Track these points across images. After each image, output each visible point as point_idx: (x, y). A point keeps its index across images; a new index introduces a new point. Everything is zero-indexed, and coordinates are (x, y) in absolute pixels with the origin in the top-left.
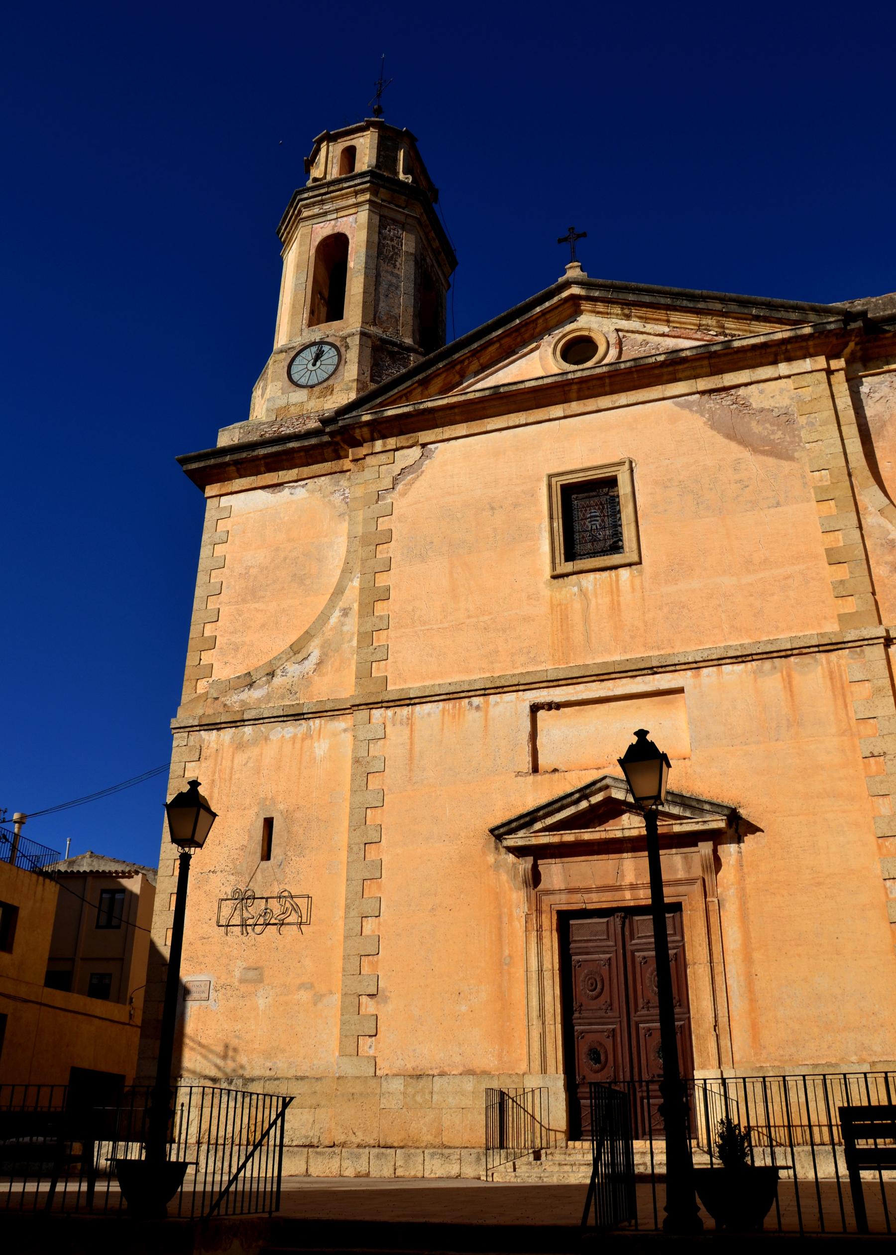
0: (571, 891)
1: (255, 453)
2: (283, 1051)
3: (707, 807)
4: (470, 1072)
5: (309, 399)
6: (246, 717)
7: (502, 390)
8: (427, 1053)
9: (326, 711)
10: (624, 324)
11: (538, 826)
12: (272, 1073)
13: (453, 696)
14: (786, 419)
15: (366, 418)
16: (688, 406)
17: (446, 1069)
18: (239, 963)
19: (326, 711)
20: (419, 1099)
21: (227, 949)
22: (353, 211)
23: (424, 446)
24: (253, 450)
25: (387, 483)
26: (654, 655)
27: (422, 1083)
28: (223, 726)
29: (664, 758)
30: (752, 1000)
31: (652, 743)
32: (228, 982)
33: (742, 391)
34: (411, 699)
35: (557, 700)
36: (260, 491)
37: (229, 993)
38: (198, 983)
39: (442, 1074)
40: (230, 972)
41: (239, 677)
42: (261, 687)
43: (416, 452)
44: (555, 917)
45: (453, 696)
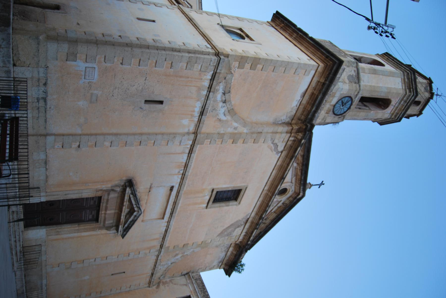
0: (108, 200)
1: (321, 94)
3: (125, 233)
4: (47, 177)
5: (331, 105)
6: (211, 93)
10: (282, 202)
11: (131, 196)
12: (48, 109)
13: (186, 166)
15: (303, 141)
18: (100, 92)
20: (37, 164)
22: (392, 112)
24: (323, 94)
25: (276, 141)
26: (176, 215)
28: (212, 82)
30: (66, 239)
33: (243, 226)
34: (191, 154)
35: (173, 193)
36: (306, 87)
38: (93, 74)
39: (46, 169)
41: (230, 88)
42: (222, 97)
43: (281, 148)
44: (99, 221)
45: (186, 166)
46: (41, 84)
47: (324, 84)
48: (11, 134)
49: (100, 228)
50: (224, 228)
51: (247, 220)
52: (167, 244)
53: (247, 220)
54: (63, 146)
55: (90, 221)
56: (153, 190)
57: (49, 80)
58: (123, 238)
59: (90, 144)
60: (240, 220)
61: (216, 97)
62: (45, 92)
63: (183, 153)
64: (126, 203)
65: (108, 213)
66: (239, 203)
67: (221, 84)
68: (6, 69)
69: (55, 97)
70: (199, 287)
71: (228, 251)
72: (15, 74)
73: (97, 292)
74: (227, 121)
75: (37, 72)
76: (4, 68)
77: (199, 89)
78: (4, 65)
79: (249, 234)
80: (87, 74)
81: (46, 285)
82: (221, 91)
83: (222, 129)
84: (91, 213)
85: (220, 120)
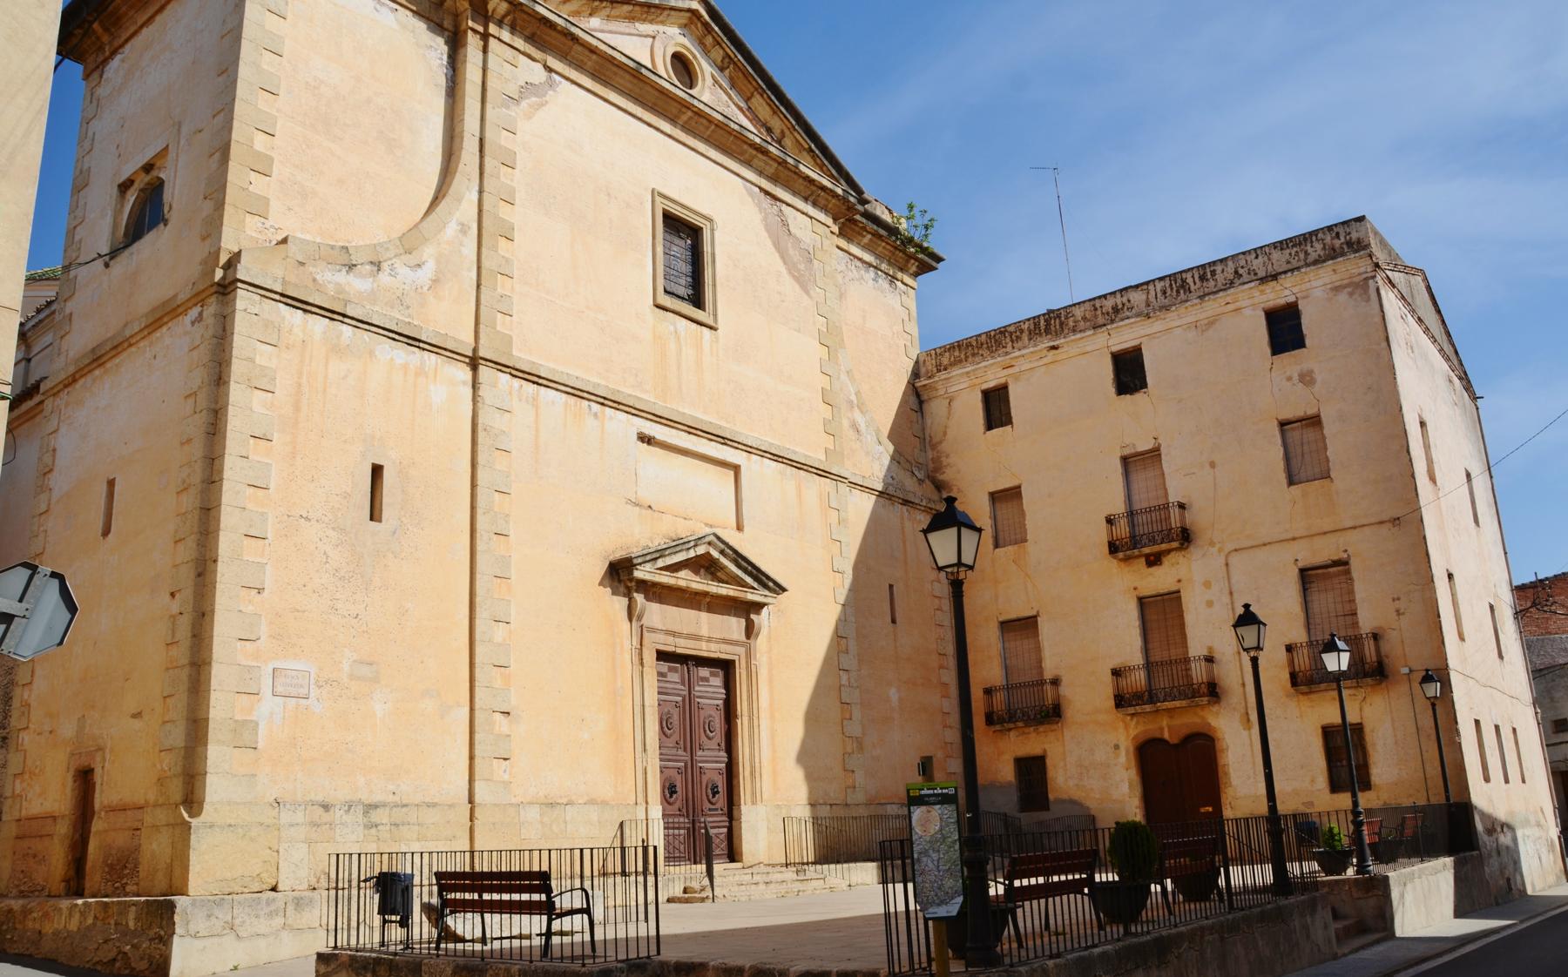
4: (592, 802)
7: (643, 71)
11: (660, 563)
12: (396, 798)
13: (577, 393)
14: (809, 256)
16: (751, 194)
23: (550, 70)
33: (784, 207)
41: (333, 247)
45: (577, 393)
46: (326, 817)
47: (875, 235)
49: (749, 655)
51: (767, 193)
52: (817, 457)
53: (767, 193)
55: (729, 684)
56: (646, 496)
57: (312, 797)
58: (784, 590)
59: (498, 683)
60: (765, 219)
62: (350, 806)
64: (686, 579)
65: (709, 632)
67: (318, 277)
68: (290, 908)
73: (941, 667)
77: (336, 350)
79: (812, 193)
80: (294, 692)
82: (342, 278)
84: (707, 680)
85: (436, 281)
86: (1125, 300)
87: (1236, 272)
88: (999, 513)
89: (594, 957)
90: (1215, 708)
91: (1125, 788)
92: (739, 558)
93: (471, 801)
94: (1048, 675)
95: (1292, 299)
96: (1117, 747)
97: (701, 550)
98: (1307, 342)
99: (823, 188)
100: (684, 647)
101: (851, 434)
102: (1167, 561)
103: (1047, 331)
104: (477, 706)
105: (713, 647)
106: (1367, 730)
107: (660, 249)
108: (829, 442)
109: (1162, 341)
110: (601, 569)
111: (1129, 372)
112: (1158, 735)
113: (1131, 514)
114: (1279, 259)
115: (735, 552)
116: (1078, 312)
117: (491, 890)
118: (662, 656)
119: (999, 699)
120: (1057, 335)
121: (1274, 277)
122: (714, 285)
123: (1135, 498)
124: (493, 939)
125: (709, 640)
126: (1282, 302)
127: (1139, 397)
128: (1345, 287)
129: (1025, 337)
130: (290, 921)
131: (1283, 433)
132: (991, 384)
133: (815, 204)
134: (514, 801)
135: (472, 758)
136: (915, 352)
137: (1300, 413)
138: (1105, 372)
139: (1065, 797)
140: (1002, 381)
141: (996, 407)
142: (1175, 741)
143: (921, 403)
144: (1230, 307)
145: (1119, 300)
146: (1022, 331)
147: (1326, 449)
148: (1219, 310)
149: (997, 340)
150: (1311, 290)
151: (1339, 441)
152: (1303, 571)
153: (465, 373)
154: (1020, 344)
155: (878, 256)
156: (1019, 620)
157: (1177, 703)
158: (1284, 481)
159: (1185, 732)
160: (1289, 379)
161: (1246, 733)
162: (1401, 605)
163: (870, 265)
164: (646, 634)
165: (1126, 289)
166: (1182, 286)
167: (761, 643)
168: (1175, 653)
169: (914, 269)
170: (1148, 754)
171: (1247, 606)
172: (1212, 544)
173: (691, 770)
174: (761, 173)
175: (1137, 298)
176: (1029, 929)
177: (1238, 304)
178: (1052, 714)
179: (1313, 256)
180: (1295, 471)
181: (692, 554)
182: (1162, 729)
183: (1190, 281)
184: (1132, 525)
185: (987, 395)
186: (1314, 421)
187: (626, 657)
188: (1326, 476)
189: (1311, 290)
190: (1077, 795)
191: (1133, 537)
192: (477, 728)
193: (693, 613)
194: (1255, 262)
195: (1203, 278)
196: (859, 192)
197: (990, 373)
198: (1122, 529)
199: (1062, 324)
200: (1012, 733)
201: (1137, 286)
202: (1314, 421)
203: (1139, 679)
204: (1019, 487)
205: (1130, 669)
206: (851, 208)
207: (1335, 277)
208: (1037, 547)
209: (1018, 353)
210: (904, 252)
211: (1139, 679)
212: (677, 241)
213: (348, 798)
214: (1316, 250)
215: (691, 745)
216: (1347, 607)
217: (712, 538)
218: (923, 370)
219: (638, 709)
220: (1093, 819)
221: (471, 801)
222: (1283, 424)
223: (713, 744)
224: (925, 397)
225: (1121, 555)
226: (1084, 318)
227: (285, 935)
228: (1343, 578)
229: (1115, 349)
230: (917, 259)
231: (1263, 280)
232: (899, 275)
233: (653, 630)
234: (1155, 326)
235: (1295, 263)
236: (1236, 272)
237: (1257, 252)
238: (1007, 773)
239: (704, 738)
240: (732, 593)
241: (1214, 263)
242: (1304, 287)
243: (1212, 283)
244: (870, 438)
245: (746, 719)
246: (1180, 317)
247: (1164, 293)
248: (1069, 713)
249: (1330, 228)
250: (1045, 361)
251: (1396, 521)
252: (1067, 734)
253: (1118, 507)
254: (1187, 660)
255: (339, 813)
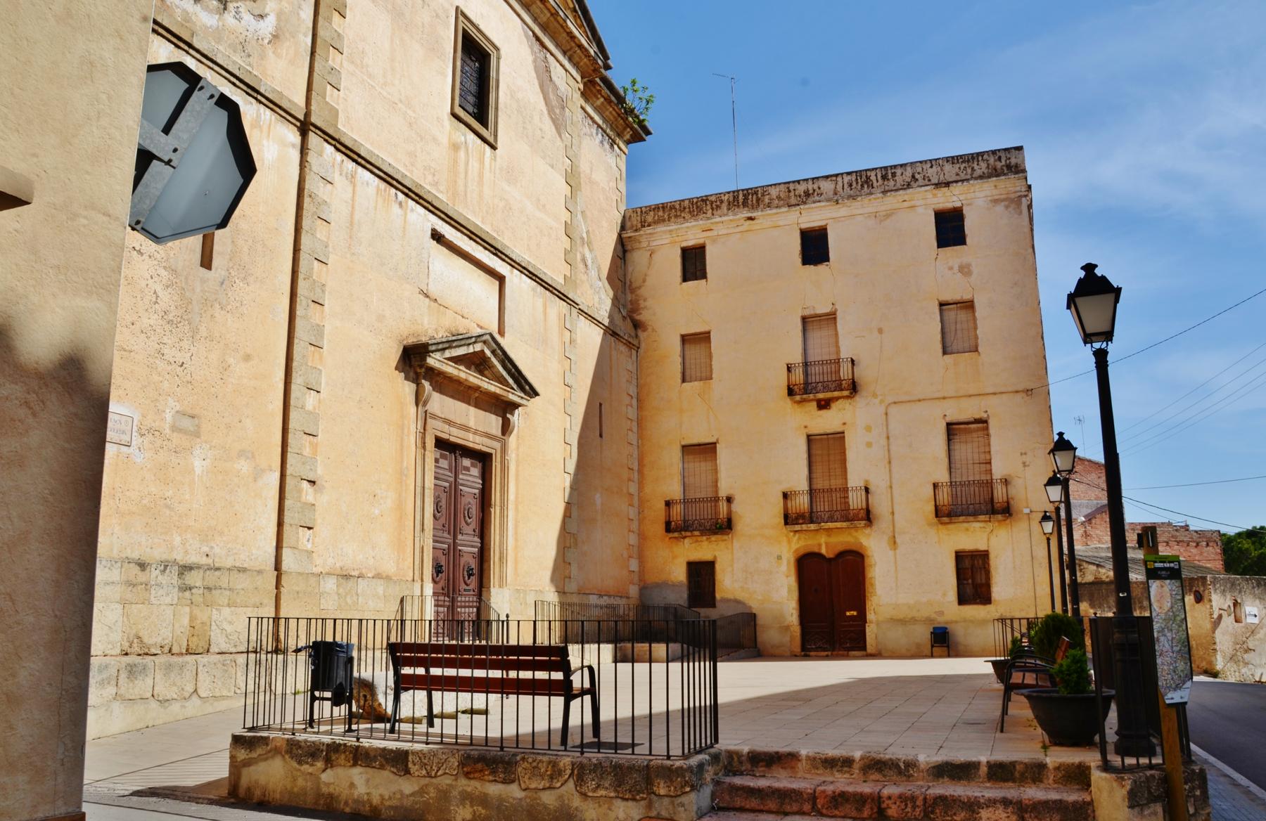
2: (221, 533)
4: (378, 576)
8: (352, 554)
9: (280, 107)
11: (448, 354)
12: (209, 561)
13: (388, 178)
16: (527, 36)
17: (364, 571)
19: (280, 107)
21: (156, 378)
27: (351, 583)
29: (1117, 292)
31: (1103, 278)
32: (156, 425)
33: (548, 55)
34: (359, 156)
37: (159, 442)
40: (160, 412)
45: (388, 178)
46: (142, 577)
48: (426, 664)
49: (504, 450)
50: (546, 112)
51: (538, 39)
52: (557, 279)
53: (538, 39)
54: (309, 528)
55: (486, 476)
56: (434, 290)
57: (129, 553)
58: (537, 394)
59: (307, 451)
60: (535, 61)
61: (207, 28)
62: (165, 566)
63: (352, 178)
64: (461, 373)
65: (474, 425)
66: (497, 49)
68: (123, 675)
69: (177, 540)
70: (664, 221)
71: (592, 118)
72: (114, 653)
73: (629, 480)
74: (279, 16)
75: (108, 588)
76: (120, 682)
78: (114, 682)
79: (571, 49)
81: (601, 596)
83: (301, 37)
84: (467, 469)
85: (275, 37)
86: (815, 186)
87: (913, 176)
88: (687, 353)
89: (633, 745)
90: (868, 531)
91: (784, 592)
92: (507, 360)
93: (278, 566)
94: (723, 493)
95: (958, 204)
96: (779, 558)
97: (478, 347)
98: (968, 240)
99: (580, 46)
100: (456, 436)
101: (581, 266)
102: (835, 406)
103: (745, 204)
104: (289, 472)
105: (478, 439)
106: (992, 556)
107: (459, 63)
108: (566, 269)
109: (844, 223)
110: (395, 355)
111: (814, 247)
112: (816, 550)
113: (806, 364)
114: (950, 171)
115: (504, 353)
116: (774, 192)
117: (438, 663)
118: (441, 444)
119: (677, 511)
120: (754, 207)
121: (947, 184)
122: (497, 108)
123: (810, 352)
124: (442, 716)
125: (476, 432)
126: (949, 205)
127: (822, 268)
128: (1003, 200)
129: (724, 206)
130: (122, 691)
131: (941, 311)
132: (690, 243)
133: (570, 60)
134: (315, 570)
135: (280, 524)
136: (623, 208)
137: (957, 297)
138: (794, 245)
139: (730, 596)
140: (701, 241)
141: (694, 263)
142: (830, 555)
143: (625, 251)
144: (906, 204)
145: (810, 186)
146: (722, 202)
147: (976, 328)
148: (898, 206)
149: (698, 206)
150: (975, 200)
151: (989, 322)
152: (948, 424)
153: (294, 137)
154: (719, 212)
155: (605, 120)
156: (699, 445)
157: (838, 525)
158: (940, 351)
159: (841, 548)
160: (951, 268)
161: (891, 553)
162: (1027, 459)
163: (599, 126)
164: (429, 420)
165: (817, 178)
166: (866, 182)
167: (512, 440)
168: (836, 483)
169: (628, 137)
170: (807, 565)
171: (1061, 434)
172: (875, 395)
173: (453, 552)
174: (535, 20)
175: (827, 186)
176: (697, 704)
177: (912, 203)
178: (725, 526)
179: (978, 172)
180: (948, 344)
181: (471, 350)
182: (820, 545)
183: (873, 178)
184: (806, 374)
185: (686, 252)
186: (969, 305)
187: (411, 440)
188: (975, 349)
189: (975, 200)
190: (741, 596)
191: (806, 383)
192: (287, 495)
193: (464, 405)
194: (930, 171)
195: (884, 177)
196: (606, 57)
197: (691, 232)
198: (798, 377)
199: (758, 200)
200: (687, 540)
201: (827, 177)
202: (969, 305)
203: (802, 503)
204: (709, 333)
205: (795, 493)
206: (596, 70)
207: (995, 192)
208: (718, 385)
209: (718, 219)
210: (625, 120)
211: (802, 503)
212: (469, 62)
213: (164, 557)
214: (981, 168)
215: (455, 532)
216: (982, 456)
217: (488, 337)
218: (628, 224)
219: (419, 490)
220: (753, 617)
221: (278, 566)
222: (941, 305)
223: (469, 530)
224: (629, 248)
225: (798, 398)
226: (779, 198)
227: (116, 706)
228: (981, 433)
229: (804, 226)
230: (632, 128)
231: (938, 185)
232: (618, 140)
233: (434, 417)
234: (841, 211)
235: (963, 176)
236: (913, 176)
237: (932, 162)
238: (679, 574)
239: (463, 523)
240: (498, 391)
241: (895, 166)
242: (969, 196)
243: (892, 183)
244: (593, 273)
245: (498, 509)
246: (863, 207)
247: (851, 185)
248: (739, 526)
249: (994, 152)
250: (740, 229)
251: (1028, 392)
252: (736, 544)
253: (797, 358)
254: (846, 490)
255: (155, 573)
